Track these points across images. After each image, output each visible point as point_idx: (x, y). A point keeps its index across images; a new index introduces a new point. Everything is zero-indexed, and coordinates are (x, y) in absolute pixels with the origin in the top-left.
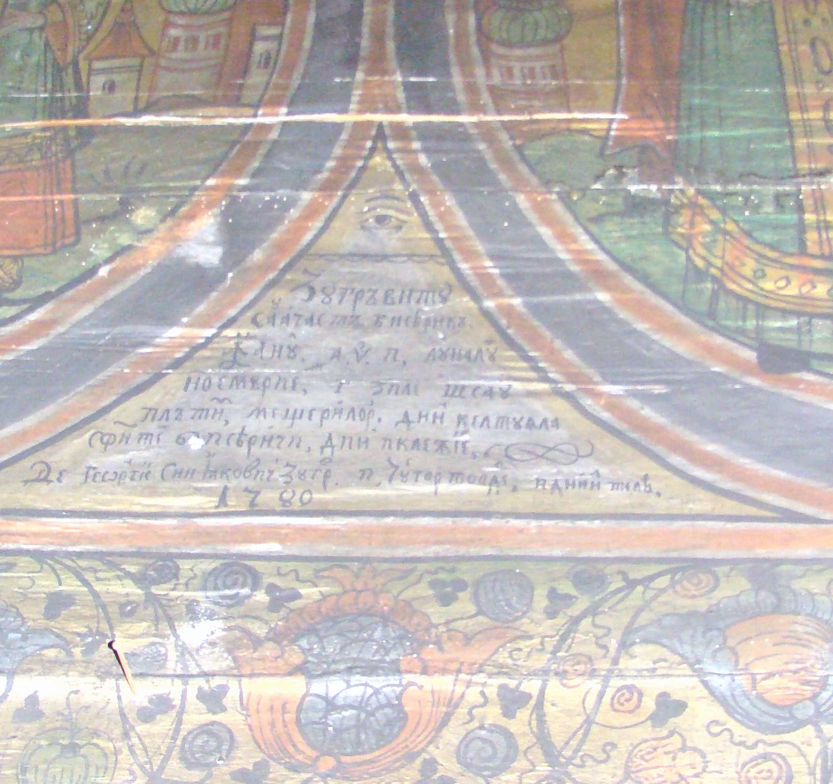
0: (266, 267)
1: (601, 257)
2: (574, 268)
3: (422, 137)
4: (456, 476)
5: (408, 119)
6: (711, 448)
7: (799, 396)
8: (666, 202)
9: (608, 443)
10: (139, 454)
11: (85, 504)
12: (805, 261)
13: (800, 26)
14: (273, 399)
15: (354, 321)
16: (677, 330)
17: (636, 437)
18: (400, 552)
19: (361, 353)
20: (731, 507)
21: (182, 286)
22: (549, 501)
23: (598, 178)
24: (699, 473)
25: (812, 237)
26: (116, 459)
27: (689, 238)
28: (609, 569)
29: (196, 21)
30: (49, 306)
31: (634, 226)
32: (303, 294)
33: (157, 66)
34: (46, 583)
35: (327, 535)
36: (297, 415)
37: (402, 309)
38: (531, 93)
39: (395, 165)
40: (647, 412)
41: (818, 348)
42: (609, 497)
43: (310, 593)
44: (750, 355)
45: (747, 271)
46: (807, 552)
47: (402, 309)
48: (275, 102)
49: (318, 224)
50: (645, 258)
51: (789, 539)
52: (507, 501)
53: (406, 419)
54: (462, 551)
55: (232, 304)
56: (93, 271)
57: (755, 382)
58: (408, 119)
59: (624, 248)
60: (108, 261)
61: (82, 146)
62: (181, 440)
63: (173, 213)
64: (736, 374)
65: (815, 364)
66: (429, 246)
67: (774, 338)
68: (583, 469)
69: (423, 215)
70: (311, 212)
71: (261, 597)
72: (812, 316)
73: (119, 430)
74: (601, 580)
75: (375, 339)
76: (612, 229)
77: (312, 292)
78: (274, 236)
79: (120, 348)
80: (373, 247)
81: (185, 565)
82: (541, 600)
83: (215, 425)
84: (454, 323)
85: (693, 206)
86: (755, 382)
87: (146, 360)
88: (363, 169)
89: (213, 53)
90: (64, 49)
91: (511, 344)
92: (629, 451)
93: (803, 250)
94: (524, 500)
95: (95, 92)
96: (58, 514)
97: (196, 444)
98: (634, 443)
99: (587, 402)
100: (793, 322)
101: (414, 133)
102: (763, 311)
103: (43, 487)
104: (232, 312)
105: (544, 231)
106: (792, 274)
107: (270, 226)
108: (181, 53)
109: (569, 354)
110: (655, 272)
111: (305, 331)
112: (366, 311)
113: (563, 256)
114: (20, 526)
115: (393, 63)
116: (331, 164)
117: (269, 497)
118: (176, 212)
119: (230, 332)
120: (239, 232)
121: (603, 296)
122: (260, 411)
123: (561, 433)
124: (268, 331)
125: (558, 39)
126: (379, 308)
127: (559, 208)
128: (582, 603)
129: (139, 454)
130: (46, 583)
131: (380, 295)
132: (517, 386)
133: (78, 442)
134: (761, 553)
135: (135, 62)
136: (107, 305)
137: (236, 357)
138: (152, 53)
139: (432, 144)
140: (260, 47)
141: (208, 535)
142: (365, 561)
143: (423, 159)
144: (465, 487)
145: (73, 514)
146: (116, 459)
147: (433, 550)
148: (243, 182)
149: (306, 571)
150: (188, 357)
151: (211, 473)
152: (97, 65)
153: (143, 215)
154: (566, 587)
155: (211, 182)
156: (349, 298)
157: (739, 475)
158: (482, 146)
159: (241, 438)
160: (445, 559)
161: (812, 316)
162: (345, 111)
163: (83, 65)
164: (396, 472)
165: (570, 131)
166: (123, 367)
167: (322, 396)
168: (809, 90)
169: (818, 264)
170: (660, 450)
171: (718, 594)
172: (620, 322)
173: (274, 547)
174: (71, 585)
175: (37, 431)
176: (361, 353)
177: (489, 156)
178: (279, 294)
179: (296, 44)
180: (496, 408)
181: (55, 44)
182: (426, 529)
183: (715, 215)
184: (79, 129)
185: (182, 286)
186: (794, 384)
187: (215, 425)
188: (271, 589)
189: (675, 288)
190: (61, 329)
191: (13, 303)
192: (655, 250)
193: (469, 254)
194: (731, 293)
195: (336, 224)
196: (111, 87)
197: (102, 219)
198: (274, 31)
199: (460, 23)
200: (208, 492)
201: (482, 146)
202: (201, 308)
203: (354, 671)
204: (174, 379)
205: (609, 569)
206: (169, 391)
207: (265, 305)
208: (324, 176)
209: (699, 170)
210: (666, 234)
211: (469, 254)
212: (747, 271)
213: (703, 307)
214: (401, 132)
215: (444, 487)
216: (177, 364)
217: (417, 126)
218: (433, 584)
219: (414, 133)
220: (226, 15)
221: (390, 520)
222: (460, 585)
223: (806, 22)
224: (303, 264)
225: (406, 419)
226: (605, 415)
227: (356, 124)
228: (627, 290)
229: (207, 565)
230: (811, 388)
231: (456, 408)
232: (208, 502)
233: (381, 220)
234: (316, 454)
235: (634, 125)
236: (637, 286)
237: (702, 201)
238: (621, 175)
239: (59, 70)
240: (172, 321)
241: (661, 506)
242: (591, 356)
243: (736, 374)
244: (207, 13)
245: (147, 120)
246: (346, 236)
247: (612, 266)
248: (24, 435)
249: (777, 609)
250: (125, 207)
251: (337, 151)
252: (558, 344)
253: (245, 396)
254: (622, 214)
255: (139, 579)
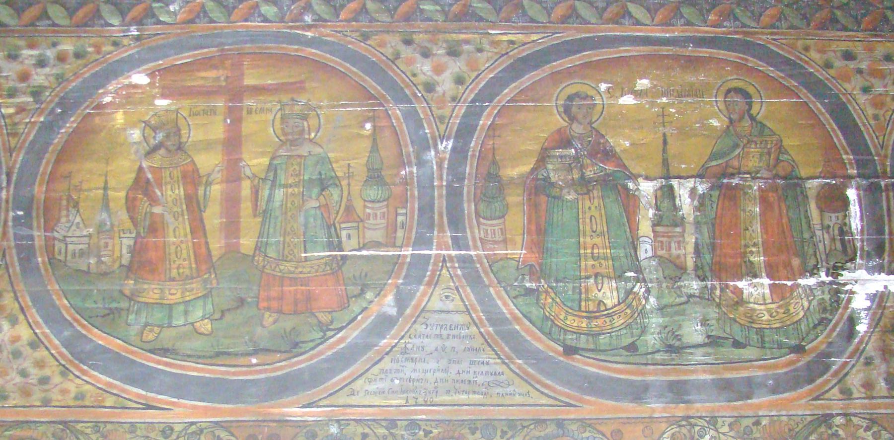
0: (411, 316)
1: (517, 311)
2: (508, 316)
3: (458, 261)
4: (474, 392)
5: (453, 253)
6: (548, 382)
7: (574, 364)
8: (537, 290)
9: (517, 380)
10: (380, 385)
11: (367, 403)
12: (580, 314)
13: (587, 210)
14: (420, 366)
15: (440, 336)
16: (539, 340)
17: (526, 378)
18: (459, 418)
19: (444, 349)
20: (552, 402)
21: (385, 323)
22: (501, 401)
23: (516, 280)
24: (543, 390)
25: (583, 304)
26: (373, 387)
27: (544, 305)
28: (518, 423)
29: (378, 205)
30: (344, 331)
31: (528, 299)
32: (424, 326)
33: (364, 227)
34: (360, 430)
35: (438, 412)
36: (426, 372)
37: (455, 332)
38: (495, 242)
39: (450, 274)
40: (530, 370)
41: (582, 345)
42: (518, 399)
43: (435, 431)
44: (561, 349)
45: (562, 317)
46: (572, 417)
47: (455, 332)
48: (407, 246)
49: (426, 299)
50: (530, 312)
51: (568, 412)
52: (489, 401)
53: (459, 373)
54: (477, 417)
55: (402, 331)
56: (356, 318)
57: (561, 359)
58: (453, 253)
59: (525, 309)
60: (360, 314)
61: (343, 264)
62: (392, 380)
63: (379, 294)
64: (556, 356)
65: (580, 352)
66: (463, 308)
67: (569, 343)
68: (510, 389)
69: (460, 295)
70: (424, 294)
71: (421, 433)
72: (581, 334)
73: (373, 377)
74: (516, 426)
75: (448, 344)
76: (520, 301)
77: (427, 325)
78: (413, 303)
79: (368, 347)
80: (445, 308)
81: (399, 423)
82: (499, 433)
83: (401, 375)
84: (472, 337)
85: (547, 292)
86: (561, 359)
87: (378, 352)
88: (440, 275)
89: (383, 221)
90: (329, 218)
91: (490, 346)
92: (523, 383)
93: (580, 310)
94: (495, 400)
95: (344, 239)
96: (359, 406)
97: (397, 382)
98: (526, 381)
99: (512, 366)
100: (575, 336)
101: (455, 260)
102: (566, 331)
103: (353, 398)
104: (403, 334)
105: (499, 302)
106: (576, 318)
107: (411, 300)
108: (372, 221)
109: (506, 349)
110: (534, 318)
111: (426, 340)
112: (445, 333)
113: (505, 311)
114: (349, 410)
115: (447, 228)
116: (428, 273)
117: (420, 400)
118: (380, 292)
119: (402, 341)
120: (401, 302)
121: (517, 327)
122: (415, 370)
123: (503, 378)
124: (414, 341)
125: (503, 217)
126: (448, 332)
127: (503, 293)
128: (510, 433)
129: (380, 385)
130: (360, 430)
131: (448, 327)
132: (491, 361)
133: (360, 382)
134: (560, 417)
135: (355, 224)
136: (363, 330)
137: (405, 351)
138: (362, 221)
139: (462, 265)
140: (400, 219)
141: (404, 413)
142: (450, 421)
143: (459, 272)
144: (477, 396)
145: (364, 406)
146: (373, 387)
147: (469, 417)
148: (401, 281)
149: (433, 424)
150: (391, 350)
151: (403, 392)
152: (343, 226)
153: (369, 295)
154: (505, 429)
155: (390, 281)
156: (439, 328)
157: (555, 391)
158: (478, 266)
159: (410, 380)
160: (471, 420)
161: (581, 334)
162: (431, 250)
163: (337, 225)
164: (457, 391)
165: (507, 258)
166: (370, 354)
167: (433, 365)
168: (588, 239)
169: (584, 314)
170: (533, 383)
171: (547, 431)
172: (522, 337)
173: (424, 417)
174: (367, 430)
175: (349, 376)
176: (444, 349)
177: (480, 270)
178: (416, 326)
179: (412, 217)
180: (485, 368)
181: (326, 215)
182: (466, 410)
183: (553, 295)
184: (342, 256)
185: (385, 323)
186: (573, 360)
187: (401, 375)
188: (424, 430)
189: (539, 324)
190: (349, 340)
191: (332, 330)
192: (533, 310)
193: (476, 311)
194: (557, 325)
195: (433, 298)
196: (349, 237)
197: (355, 296)
198: (404, 211)
199: (469, 206)
200: (401, 398)
201: (478, 266)
202: (393, 332)
203: (91, 15)
204: (387, 359)
205: (518, 423)
206: (386, 364)
207: (412, 330)
208: (427, 279)
209: (550, 276)
210: (537, 303)
211: (476, 311)
212: (562, 317)
213: (547, 331)
214: (451, 258)
215: (471, 396)
216: (387, 354)
217: (456, 256)
218: (470, 428)
219: (455, 260)
220: (385, 203)
221: (456, 407)
222: (477, 429)
223: (590, 208)
224: (423, 314)
225: (459, 373)
226: (517, 371)
227: (436, 255)
228: (525, 324)
229: (406, 423)
230: (578, 361)
231: (474, 368)
232: (403, 402)
233: (447, 297)
234: (433, 385)
235: (529, 256)
236: (528, 323)
237: (550, 290)
238: (523, 279)
239: (329, 227)
240: (384, 338)
241: (531, 401)
242: (515, 350)
243: (556, 356)
244: (379, 202)
245: (364, 253)
246: (436, 303)
247: (520, 315)
248: (344, 379)
249: (563, 435)
250: (363, 292)
251: (430, 268)
252: (503, 345)
253: (410, 365)
254: (525, 295)
255: (387, 428)
